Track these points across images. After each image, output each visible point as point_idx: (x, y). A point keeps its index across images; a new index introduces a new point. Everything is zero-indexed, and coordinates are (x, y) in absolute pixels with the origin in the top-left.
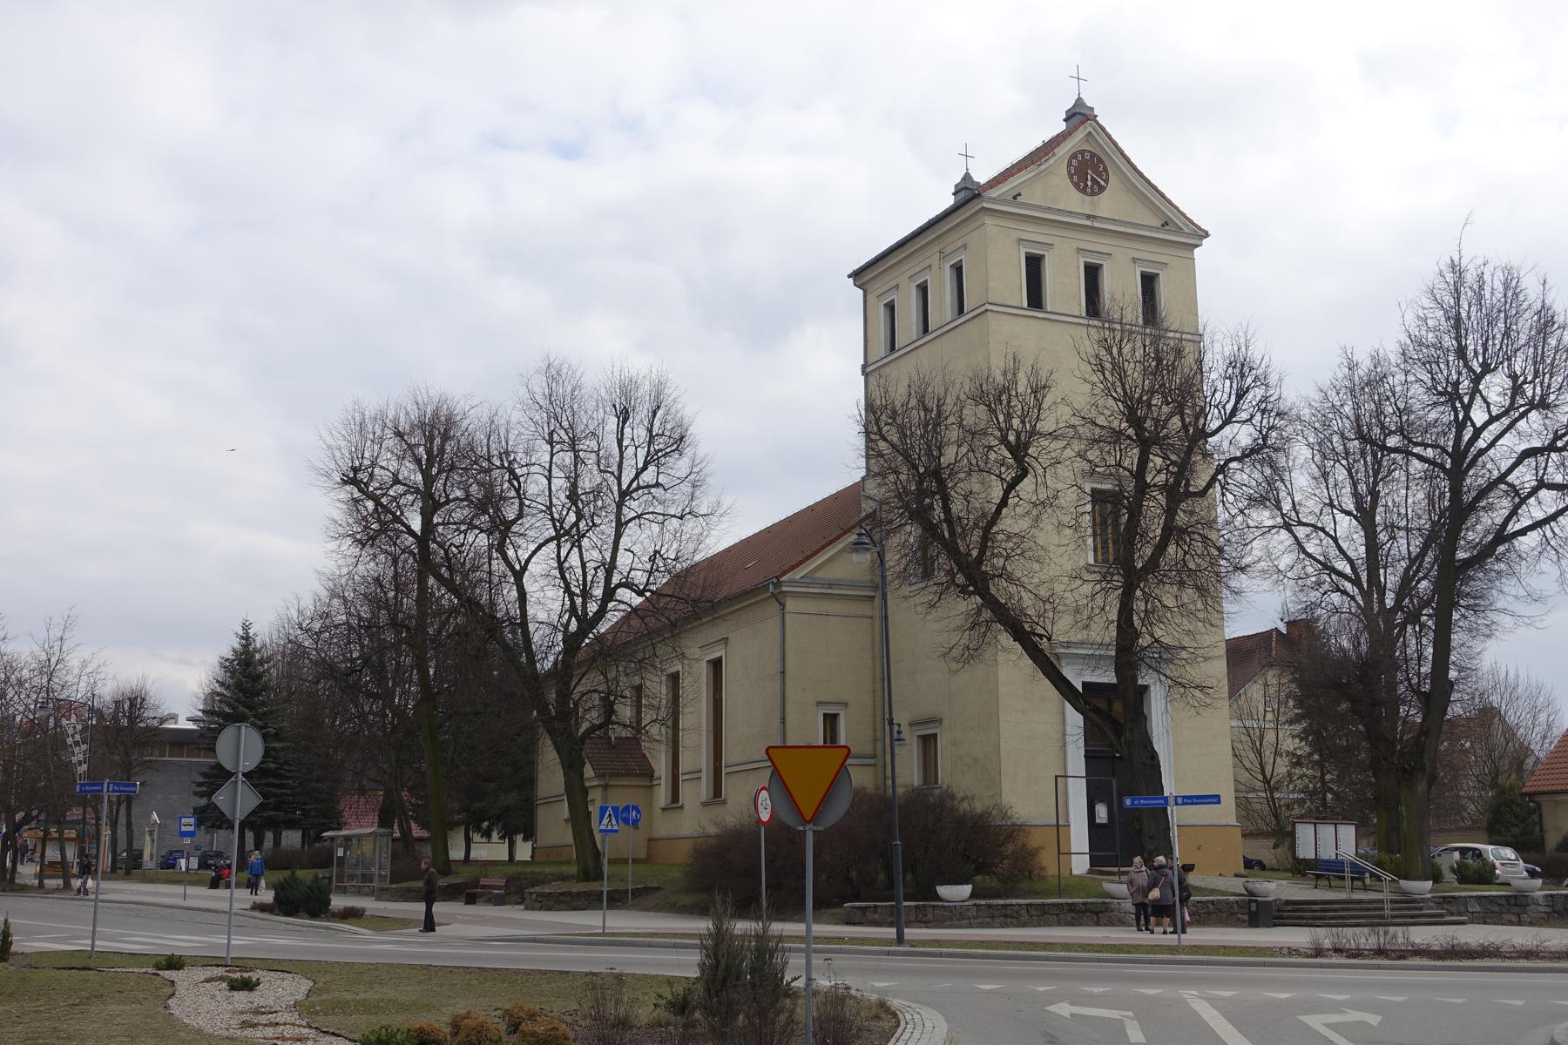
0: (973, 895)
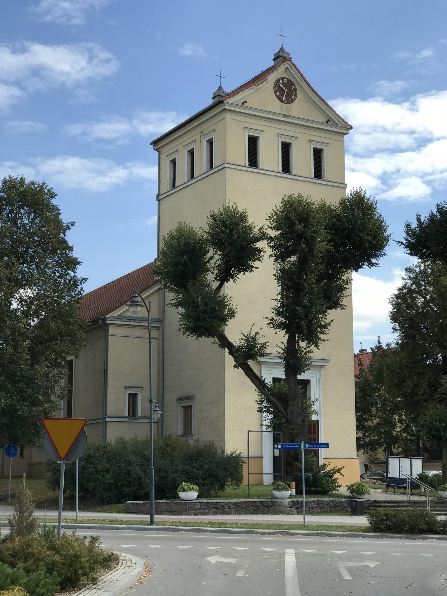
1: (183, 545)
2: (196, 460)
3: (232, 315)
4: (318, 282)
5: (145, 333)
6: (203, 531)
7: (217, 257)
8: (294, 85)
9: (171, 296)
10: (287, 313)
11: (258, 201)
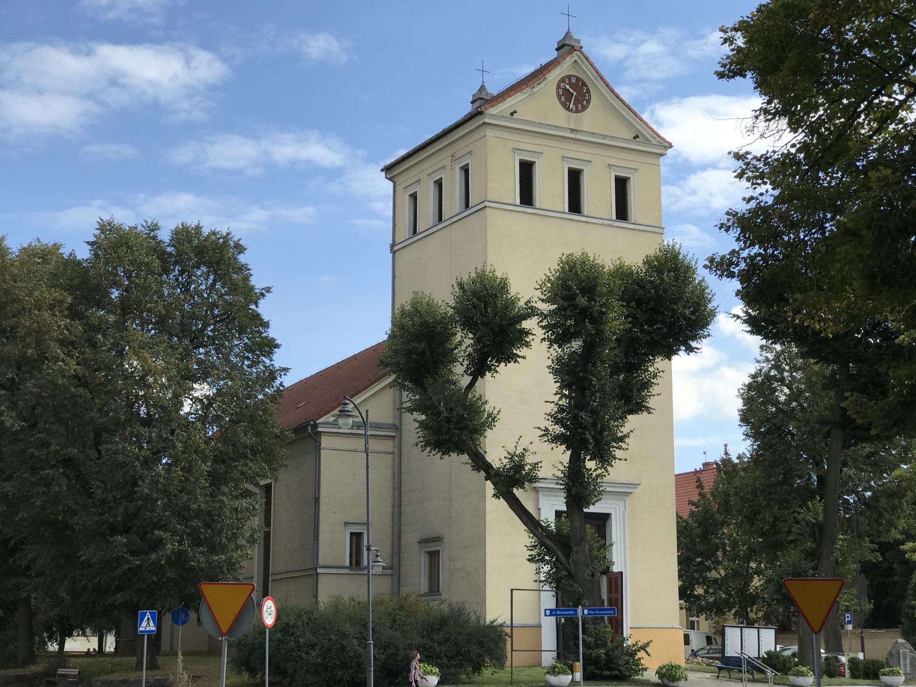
2: (439, 630)
3: (492, 419)
8: (585, 85)
10: (568, 420)
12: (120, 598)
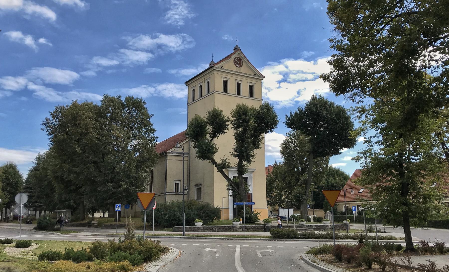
0: (203, 225)
1: (196, 244)
3: (217, 151)
4: (251, 138)
5: (182, 158)
6: (204, 238)
7: (211, 128)
9: (192, 144)
11: (227, 106)
12: (109, 201)
